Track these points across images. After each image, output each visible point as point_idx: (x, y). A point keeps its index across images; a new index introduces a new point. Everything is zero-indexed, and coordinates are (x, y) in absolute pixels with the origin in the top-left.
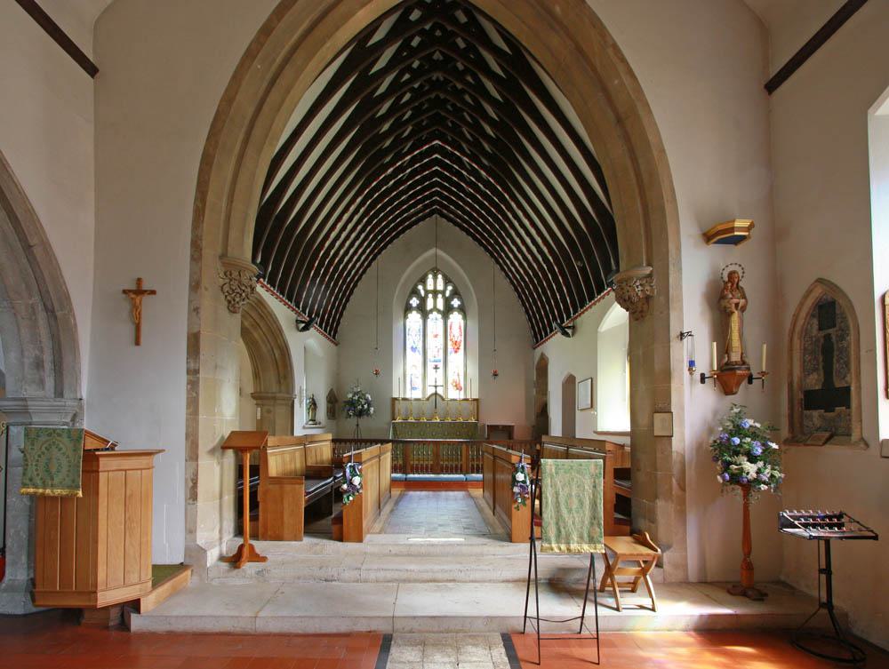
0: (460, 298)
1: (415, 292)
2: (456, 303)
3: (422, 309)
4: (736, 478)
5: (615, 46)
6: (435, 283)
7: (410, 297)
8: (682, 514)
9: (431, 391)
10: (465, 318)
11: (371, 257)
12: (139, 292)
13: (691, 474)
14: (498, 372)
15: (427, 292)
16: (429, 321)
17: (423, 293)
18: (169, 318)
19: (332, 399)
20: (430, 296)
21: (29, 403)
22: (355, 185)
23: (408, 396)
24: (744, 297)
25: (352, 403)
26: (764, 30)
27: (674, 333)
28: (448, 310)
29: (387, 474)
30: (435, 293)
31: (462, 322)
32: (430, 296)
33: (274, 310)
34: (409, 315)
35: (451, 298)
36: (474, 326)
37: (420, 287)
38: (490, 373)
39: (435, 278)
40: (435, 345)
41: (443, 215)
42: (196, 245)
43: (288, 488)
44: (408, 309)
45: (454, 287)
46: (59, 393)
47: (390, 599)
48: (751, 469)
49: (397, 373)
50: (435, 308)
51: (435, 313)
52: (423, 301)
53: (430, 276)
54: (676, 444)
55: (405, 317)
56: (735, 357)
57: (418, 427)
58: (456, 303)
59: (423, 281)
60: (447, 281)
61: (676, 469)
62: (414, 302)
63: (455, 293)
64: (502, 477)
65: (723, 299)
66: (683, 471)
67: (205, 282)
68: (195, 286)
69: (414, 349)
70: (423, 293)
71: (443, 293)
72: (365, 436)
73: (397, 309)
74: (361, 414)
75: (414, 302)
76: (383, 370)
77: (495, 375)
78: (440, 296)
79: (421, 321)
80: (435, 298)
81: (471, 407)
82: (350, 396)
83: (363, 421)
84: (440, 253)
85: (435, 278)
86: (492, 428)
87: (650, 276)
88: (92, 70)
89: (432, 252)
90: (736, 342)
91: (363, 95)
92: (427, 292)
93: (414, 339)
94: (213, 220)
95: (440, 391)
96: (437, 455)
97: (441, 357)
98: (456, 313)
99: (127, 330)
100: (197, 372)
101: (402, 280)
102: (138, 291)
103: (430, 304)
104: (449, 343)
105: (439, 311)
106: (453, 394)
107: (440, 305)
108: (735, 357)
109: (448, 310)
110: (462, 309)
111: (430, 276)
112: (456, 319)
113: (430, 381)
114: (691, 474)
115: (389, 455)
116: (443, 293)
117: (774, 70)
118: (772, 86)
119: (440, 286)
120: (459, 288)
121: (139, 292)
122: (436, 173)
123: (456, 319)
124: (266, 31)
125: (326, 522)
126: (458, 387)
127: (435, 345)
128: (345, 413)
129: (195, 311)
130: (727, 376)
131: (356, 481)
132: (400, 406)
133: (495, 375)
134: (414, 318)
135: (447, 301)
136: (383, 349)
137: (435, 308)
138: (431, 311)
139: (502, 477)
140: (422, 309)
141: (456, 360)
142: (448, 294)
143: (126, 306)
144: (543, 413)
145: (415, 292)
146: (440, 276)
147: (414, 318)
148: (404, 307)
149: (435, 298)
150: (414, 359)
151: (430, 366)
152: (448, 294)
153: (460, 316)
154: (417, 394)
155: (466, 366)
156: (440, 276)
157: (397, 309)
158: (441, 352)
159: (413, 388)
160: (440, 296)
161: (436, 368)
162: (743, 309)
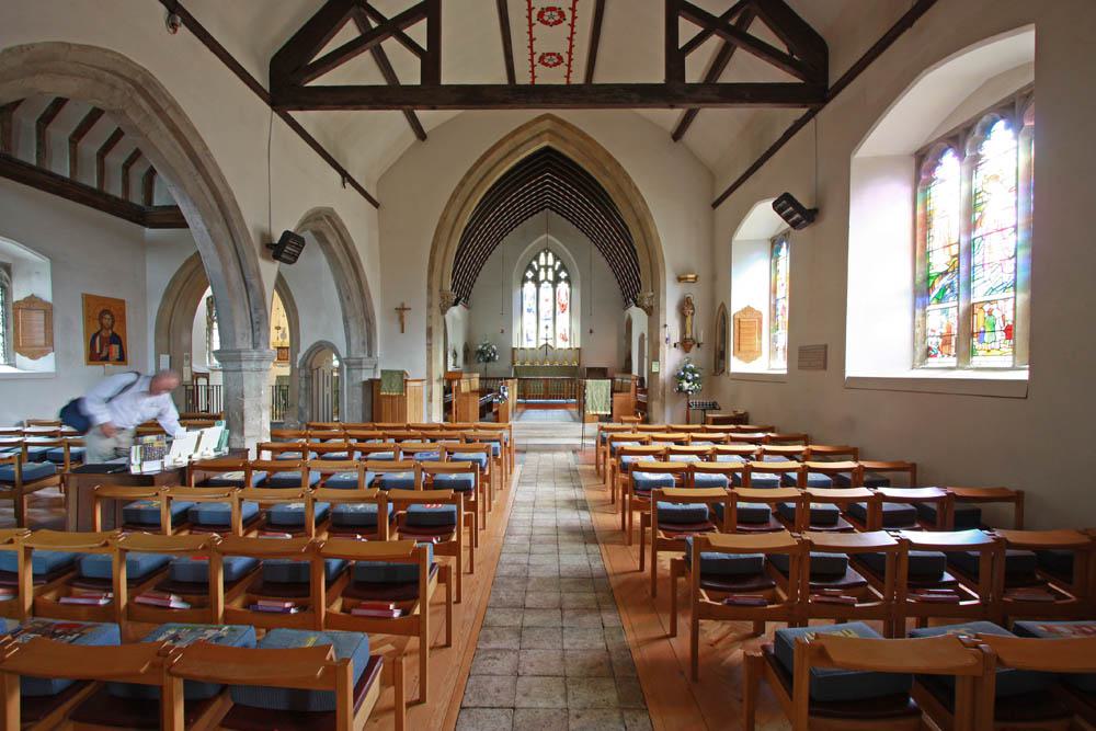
0: (566, 271)
1: (530, 267)
2: (563, 275)
3: (536, 280)
4: (681, 389)
5: (636, 188)
6: (546, 259)
7: (526, 271)
8: (663, 407)
9: (543, 342)
10: (570, 286)
12: (404, 309)
13: (668, 390)
14: (595, 330)
15: (540, 267)
16: (541, 290)
17: (536, 267)
18: (418, 320)
19: (467, 350)
20: (542, 269)
21: (243, 354)
22: (553, 403)
23: (524, 346)
24: (693, 309)
25: (482, 353)
26: (712, 176)
27: (662, 324)
28: (556, 281)
29: (516, 400)
30: (546, 267)
31: (568, 290)
32: (542, 269)
34: (526, 285)
35: (560, 271)
36: (577, 292)
37: (534, 263)
38: (588, 331)
39: (546, 255)
40: (546, 307)
41: (551, 209)
42: (430, 287)
43: (471, 398)
44: (525, 280)
46: (370, 356)
48: (686, 385)
49: (516, 330)
51: (546, 283)
52: (537, 273)
53: (542, 255)
54: (661, 376)
55: (522, 286)
56: (688, 336)
57: (533, 369)
58: (563, 275)
59: (537, 258)
60: (556, 258)
61: (661, 387)
62: (530, 274)
63: (563, 267)
65: (685, 307)
66: (664, 389)
67: (434, 304)
68: (430, 306)
69: (529, 311)
70: (536, 267)
71: (553, 267)
72: (491, 376)
73: (516, 280)
74: (488, 360)
75: (530, 274)
76: (506, 330)
77: (591, 332)
78: (550, 270)
79: (535, 289)
80: (546, 271)
81: (574, 355)
82: (480, 347)
83: (490, 365)
84: (550, 237)
85: (546, 255)
86: (590, 370)
87: (652, 297)
88: (376, 205)
89: (545, 236)
90: (689, 329)
92: (540, 267)
93: (529, 302)
94: (436, 277)
95: (550, 343)
96: (546, 387)
97: (551, 315)
98: (563, 282)
99: (397, 327)
100: (431, 345)
101: (520, 258)
102: (401, 310)
103: (542, 276)
104: (558, 306)
105: (549, 282)
106: (562, 345)
107: (551, 277)
108: (688, 336)
109: (556, 281)
110: (568, 280)
111: (542, 255)
112: (563, 287)
113: (543, 333)
114: (668, 390)
115: (516, 386)
116: (553, 267)
117: (717, 197)
118: (715, 205)
119: (550, 262)
121: (404, 309)
122: (547, 183)
123: (563, 287)
124: (462, 184)
125: (489, 415)
126: (564, 339)
127: (546, 307)
128: (476, 360)
129: (430, 317)
130: (685, 344)
131: (506, 394)
132: (517, 354)
134: (529, 287)
135: (556, 274)
136: (506, 312)
138: (543, 281)
140: (536, 280)
141: (563, 319)
142: (556, 268)
143: (397, 316)
144: (629, 359)
145: (530, 267)
146: (550, 255)
147: (529, 287)
149: (546, 271)
150: (529, 318)
151: (543, 324)
152: (556, 268)
153: (567, 285)
154: (532, 345)
155: (570, 323)
156: (550, 255)
157: (516, 280)
158: (551, 312)
159: (529, 340)
160: (550, 270)
161: (547, 327)
162: (693, 314)
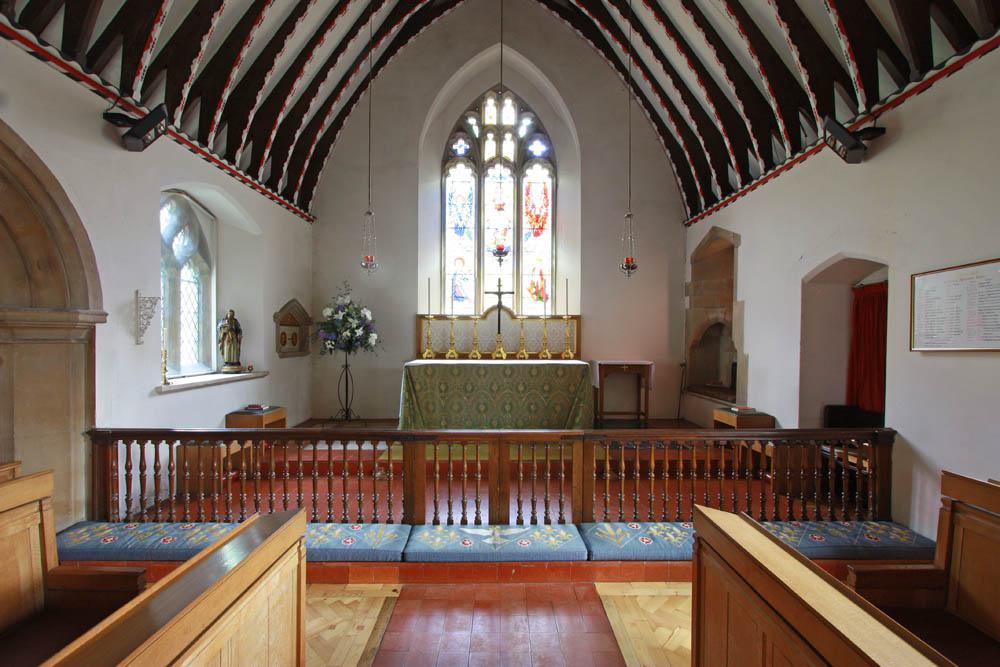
7: (453, 138)
30: (499, 131)
50: (499, 158)
52: (477, 145)
58: (538, 148)
71: (514, 130)
77: (630, 266)
105: (506, 163)
137: (499, 158)
138: (492, 163)
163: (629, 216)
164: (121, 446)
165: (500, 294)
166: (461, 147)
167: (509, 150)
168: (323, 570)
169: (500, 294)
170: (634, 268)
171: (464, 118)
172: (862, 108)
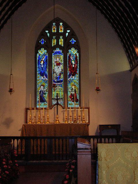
7: (40, 38)
11: (9, 12)
30: (58, 35)
33: (23, 118)
45: (71, 30)
47: (16, 143)
50: (58, 45)
51: (58, 50)
52: (50, 40)
58: (73, 41)
64: (83, 105)
71: (63, 34)
77: (98, 90)
91: (133, 8)
105: (60, 47)
120: (68, 23)
133: (98, 90)
137: (58, 45)
138: (55, 48)
139: (83, 105)
148: (34, 45)
163: (97, 73)
164: (32, 140)
165: (57, 99)
166: (42, 42)
167: (61, 42)
168: (76, 55)
169: (57, 99)
170: (99, 90)
171: (44, 30)
172: (134, 64)
